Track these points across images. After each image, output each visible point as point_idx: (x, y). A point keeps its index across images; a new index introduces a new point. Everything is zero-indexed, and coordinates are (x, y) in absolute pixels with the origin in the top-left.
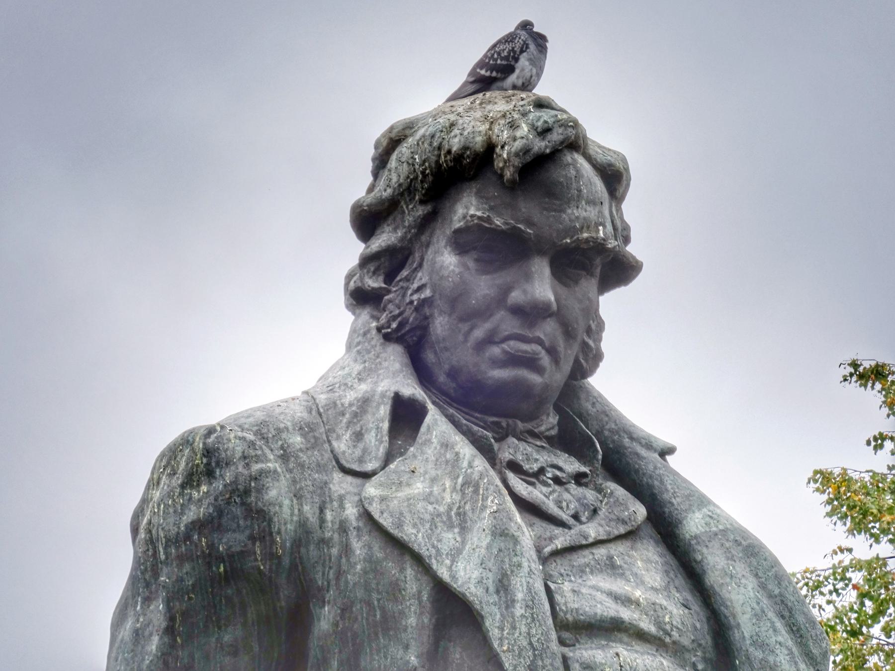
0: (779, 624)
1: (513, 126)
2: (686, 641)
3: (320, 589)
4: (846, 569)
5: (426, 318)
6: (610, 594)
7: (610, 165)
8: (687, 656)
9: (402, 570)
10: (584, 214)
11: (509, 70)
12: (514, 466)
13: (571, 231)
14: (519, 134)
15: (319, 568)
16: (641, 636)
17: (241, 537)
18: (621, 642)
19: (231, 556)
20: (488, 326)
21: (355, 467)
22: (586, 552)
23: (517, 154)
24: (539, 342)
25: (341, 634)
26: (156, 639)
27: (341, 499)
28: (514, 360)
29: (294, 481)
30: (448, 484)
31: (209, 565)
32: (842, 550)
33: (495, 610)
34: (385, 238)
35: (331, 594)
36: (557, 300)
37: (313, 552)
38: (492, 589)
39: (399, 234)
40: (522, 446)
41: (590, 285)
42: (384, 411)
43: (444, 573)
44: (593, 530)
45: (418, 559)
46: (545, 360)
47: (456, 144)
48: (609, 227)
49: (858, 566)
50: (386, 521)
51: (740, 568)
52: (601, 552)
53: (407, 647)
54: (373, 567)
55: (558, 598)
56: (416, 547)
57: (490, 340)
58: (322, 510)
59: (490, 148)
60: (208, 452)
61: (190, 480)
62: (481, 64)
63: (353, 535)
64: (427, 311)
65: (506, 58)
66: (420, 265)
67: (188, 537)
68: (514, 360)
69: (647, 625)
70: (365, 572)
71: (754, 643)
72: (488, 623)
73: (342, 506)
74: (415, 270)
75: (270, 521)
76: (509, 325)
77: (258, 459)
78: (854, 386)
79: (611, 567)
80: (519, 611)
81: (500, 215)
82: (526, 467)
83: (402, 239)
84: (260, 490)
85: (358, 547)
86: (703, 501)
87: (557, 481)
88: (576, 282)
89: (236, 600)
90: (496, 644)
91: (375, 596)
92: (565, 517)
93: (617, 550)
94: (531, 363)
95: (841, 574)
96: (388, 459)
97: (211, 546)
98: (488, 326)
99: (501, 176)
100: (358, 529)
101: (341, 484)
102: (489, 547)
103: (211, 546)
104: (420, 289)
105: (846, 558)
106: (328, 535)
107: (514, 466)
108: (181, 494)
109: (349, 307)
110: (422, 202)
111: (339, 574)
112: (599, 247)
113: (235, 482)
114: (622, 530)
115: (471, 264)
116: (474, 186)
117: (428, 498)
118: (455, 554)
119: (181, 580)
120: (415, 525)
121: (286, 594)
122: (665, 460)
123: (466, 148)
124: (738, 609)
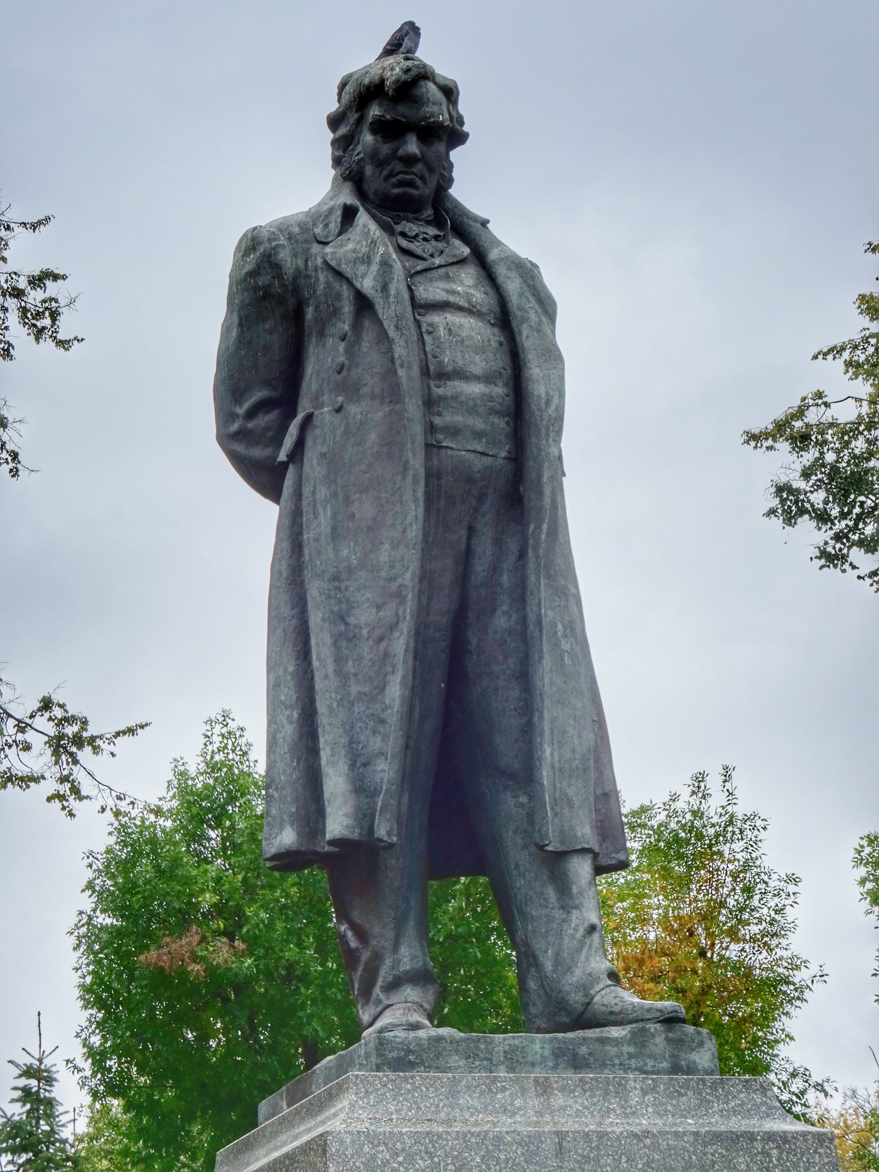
0: (531, 298)
1: (392, 69)
2: (484, 310)
3: (307, 299)
4: (868, 338)
5: (362, 167)
6: (444, 290)
7: (446, 86)
8: (485, 317)
9: (341, 286)
10: (431, 110)
11: (399, 45)
12: (403, 235)
13: (425, 118)
14: (394, 73)
15: (306, 289)
16: (460, 309)
17: (269, 277)
18: (450, 312)
19: (264, 287)
20: (389, 168)
21: (324, 240)
22: (434, 271)
23: (393, 83)
24: (415, 174)
25: (316, 320)
26: (235, 330)
27: (316, 255)
28: (401, 184)
29: (294, 249)
30: (364, 244)
31: (255, 292)
32: (864, 329)
33: (381, 300)
34: (343, 130)
35: (311, 302)
36: (421, 152)
37: (302, 282)
38: (379, 290)
39: (348, 128)
40: (409, 224)
41: (441, 147)
42: (339, 213)
43: (358, 285)
44: (437, 261)
46: (419, 182)
47: (366, 81)
48: (447, 116)
49: (872, 336)
50: (333, 263)
51: (513, 274)
52: (442, 271)
53: (344, 322)
55: (416, 293)
56: (346, 275)
57: (390, 175)
58: (306, 262)
59: (382, 81)
60: (253, 239)
61: (246, 253)
62: (388, 44)
63: (319, 271)
64: (362, 164)
65: (399, 40)
66: (358, 143)
67: (245, 280)
68: (401, 184)
69: (463, 303)
70: (324, 288)
71: (518, 308)
72: (377, 307)
73: (316, 259)
74: (356, 145)
75: (281, 269)
76: (398, 166)
77: (275, 239)
78: (870, 254)
79: (447, 277)
80: (392, 299)
81: (389, 114)
82: (409, 234)
83: (349, 131)
84: (276, 254)
85: (322, 277)
86: (499, 243)
87: (425, 239)
88: (432, 144)
89: (269, 308)
90: (381, 316)
91: (329, 300)
92: (425, 255)
93: (451, 270)
94: (411, 184)
95: (865, 340)
96: (340, 234)
97: (256, 283)
98: (389, 168)
99: (388, 94)
100: (322, 268)
101: (315, 248)
102: (378, 270)
103: (256, 283)
104: (358, 154)
105: (867, 333)
106: (309, 273)
107: (403, 235)
108: (242, 260)
109: (333, 167)
110: (356, 112)
111: (315, 291)
112: (440, 126)
113: (264, 252)
114: (455, 260)
115: (379, 139)
116: (377, 101)
117: (354, 251)
118: (364, 276)
119: (243, 300)
120: (346, 264)
121: (291, 302)
122: (487, 228)
123: (371, 83)
124: (511, 293)
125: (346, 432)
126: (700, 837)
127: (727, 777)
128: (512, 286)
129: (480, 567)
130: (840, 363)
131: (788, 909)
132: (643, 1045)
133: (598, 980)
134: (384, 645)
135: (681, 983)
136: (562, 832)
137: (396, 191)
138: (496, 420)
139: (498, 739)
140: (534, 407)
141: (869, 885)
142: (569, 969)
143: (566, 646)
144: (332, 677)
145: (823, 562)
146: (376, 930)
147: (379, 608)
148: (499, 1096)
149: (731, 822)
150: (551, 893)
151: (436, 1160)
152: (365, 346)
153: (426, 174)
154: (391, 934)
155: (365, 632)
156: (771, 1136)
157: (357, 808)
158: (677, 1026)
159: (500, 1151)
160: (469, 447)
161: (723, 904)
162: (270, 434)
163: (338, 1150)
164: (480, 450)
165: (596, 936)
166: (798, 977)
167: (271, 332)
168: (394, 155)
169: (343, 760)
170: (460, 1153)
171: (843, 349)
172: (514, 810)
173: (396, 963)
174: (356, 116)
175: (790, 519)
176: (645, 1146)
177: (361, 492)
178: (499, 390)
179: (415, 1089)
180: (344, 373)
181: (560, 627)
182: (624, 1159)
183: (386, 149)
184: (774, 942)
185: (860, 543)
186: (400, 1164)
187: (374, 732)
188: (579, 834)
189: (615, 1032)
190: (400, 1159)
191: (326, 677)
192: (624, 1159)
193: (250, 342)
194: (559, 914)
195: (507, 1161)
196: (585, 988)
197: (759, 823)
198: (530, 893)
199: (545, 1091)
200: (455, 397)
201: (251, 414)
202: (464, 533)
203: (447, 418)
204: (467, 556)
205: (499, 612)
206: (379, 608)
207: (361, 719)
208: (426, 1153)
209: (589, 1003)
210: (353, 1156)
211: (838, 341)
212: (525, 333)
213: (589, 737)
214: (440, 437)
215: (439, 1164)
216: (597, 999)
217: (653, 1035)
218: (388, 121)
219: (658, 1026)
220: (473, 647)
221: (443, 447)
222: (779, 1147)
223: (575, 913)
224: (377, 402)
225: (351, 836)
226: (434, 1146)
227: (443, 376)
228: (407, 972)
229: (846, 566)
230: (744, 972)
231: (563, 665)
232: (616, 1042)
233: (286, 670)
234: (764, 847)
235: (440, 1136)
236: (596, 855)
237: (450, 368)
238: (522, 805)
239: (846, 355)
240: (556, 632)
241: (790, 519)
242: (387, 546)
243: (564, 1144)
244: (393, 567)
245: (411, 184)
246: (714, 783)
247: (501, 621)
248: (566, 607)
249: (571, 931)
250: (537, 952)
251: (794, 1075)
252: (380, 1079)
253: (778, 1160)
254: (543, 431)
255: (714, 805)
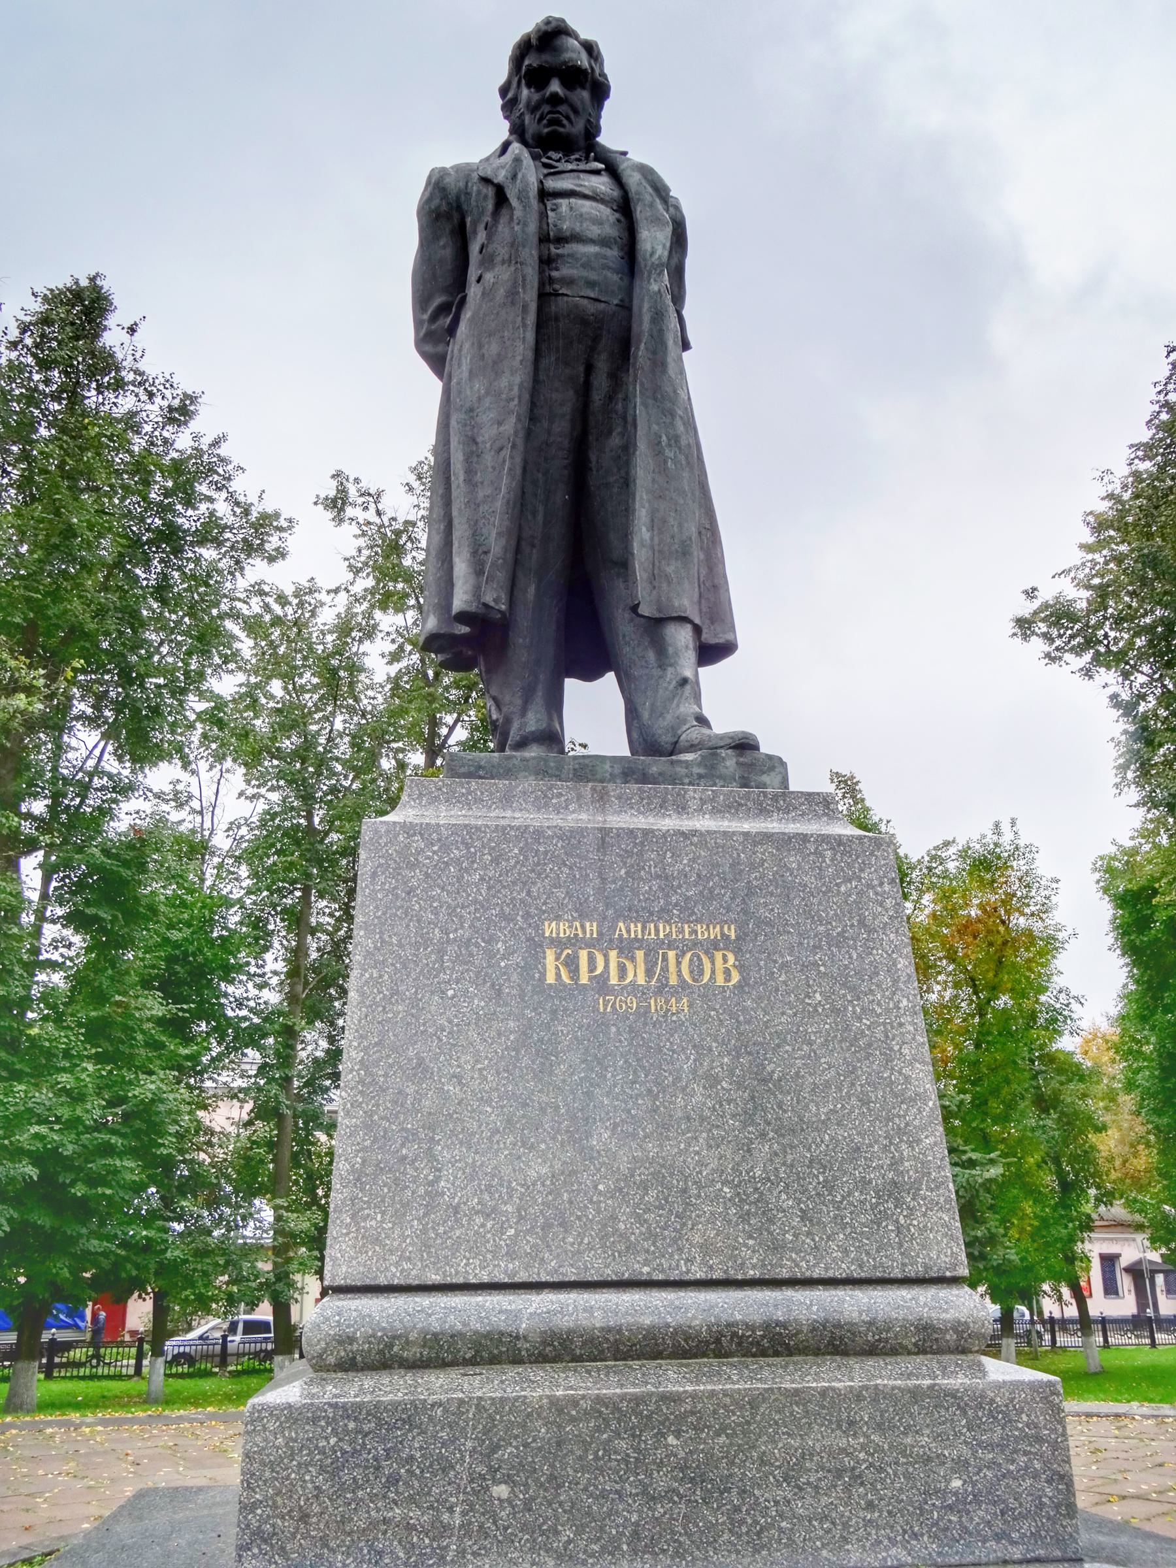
13: (565, 63)
43: (496, 181)
46: (565, 122)
95: (1083, 564)
125: (483, 294)
126: (999, 858)
127: (1013, 823)
128: (633, 180)
129: (597, 397)
130: (1069, 579)
131: (1053, 897)
132: (713, 767)
133: (685, 722)
135: (990, 938)
136: (659, 602)
138: (609, 274)
139: (612, 536)
141: (1102, 884)
142: (661, 715)
143: (669, 453)
144: (462, 485)
145: (1047, 660)
146: (507, 698)
148: (554, 801)
149: (1017, 848)
150: (651, 655)
151: (472, 850)
152: (500, 228)
153: (572, 116)
154: (519, 702)
155: (488, 445)
156: (824, 839)
158: (748, 752)
159: (540, 843)
160: (582, 294)
161: (1014, 895)
163: (371, 839)
164: (592, 295)
165: (688, 688)
166: (1061, 936)
167: (444, 247)
169: (467, 549)
170: (498, 845)
171: (1070, 571)
173: (523, 725)
175: (1025, 637)
176: (692, 844)
178: (613, 253)
179: (469, 793)
181: (664, 438)
182: (669, 854)
184: (1044, 916)
185: (1072, 650)
186: (434, 852)
188: (676, 604)
189: (689, 757)
190: (435, 848)
191: (458, 486)
192: (669, 854)
194: (656, 672)
195: (546, 853)
196: (673, 729)
197: (1034, 849)
198: (634, 657)
199: (602, 798)
200: (571, 255)
202: (582, 369)
203: (565, 271)
204: (585, 390)
206: (500, 423)
207: (484, 517)
208: (462, 843)
209: (676, 742)
210: (386, 845)
211: (1067, 567)
212: (639, 209)
213: (544, 363)
214: (557, 286)
215: (475, 854)
216: (683, 737)
217: (724, 759)
219: (729, 751)
220: (593, 464)
221: (559, 295)
222: (832, 849)
223: (670, 670)
225: (468, 609)
226: (471, 838)
227: (561, 240)
228: (533, 733)
229: (1062, 663)
230: (1029, 933)
231: (666, 469)
232: (687, 764)
234: (1037, 863)
235: (478, 828)
236: (697, 630)
237: (568, 234)
239: (1072, 574)
240: (660, 442)
241: (1025, 637)
243: (607, 839)
244: (511, 390)
245: (558, 123)
246: (1005, 827)
247: (615, 441)
248: (672, 424)
249: (665, 685)
251: (1060, 992)
252: (435, 783)
253: (832, 860)
254: (646, 275)
255: (1007, 838)
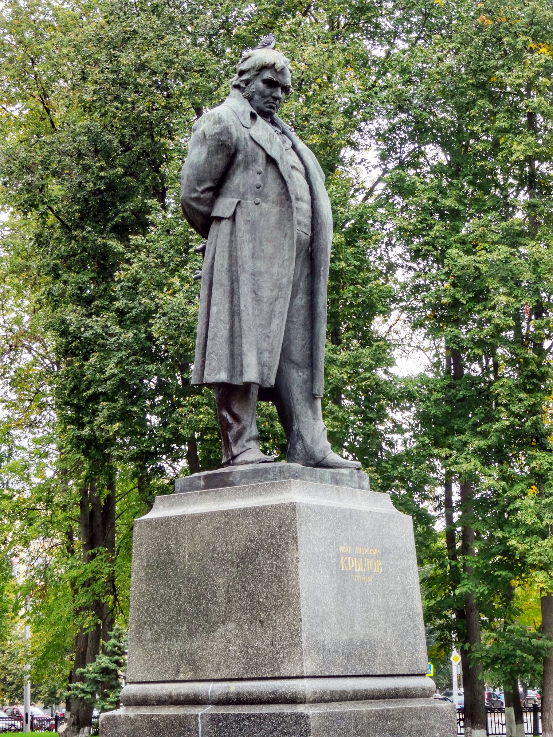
43: (269, 153)
45: (263, 149)
54: (253, 149)
57: (267, 102)
60: (219, 118)
67: (214, 135)
76: (272, 100)
121: (233, 150)
134: (272, 307)
137: (267, 109)
140: (323, 218)
146: (245, 418)
147: (272, 291)
150: (310, 412)
155: (265, 299)
157: (259, 370)
162: (208, 201)
168: (270, 95)
172: (297, 378)
173: (251, 432)
174: (256, 73)
177: (267, 241)
180: (261, 189)
183: (268, 91)
187: (265, 341)
189: (343, 471)
193: (210, 162)
194: (312, 421)
201: (203, 192)
205: (298, 297)
218: (273, 81)
224: (275, 205)
233: (224, 307)
238: (300, 376)
242: (276, 266)
250: (304, 435)
